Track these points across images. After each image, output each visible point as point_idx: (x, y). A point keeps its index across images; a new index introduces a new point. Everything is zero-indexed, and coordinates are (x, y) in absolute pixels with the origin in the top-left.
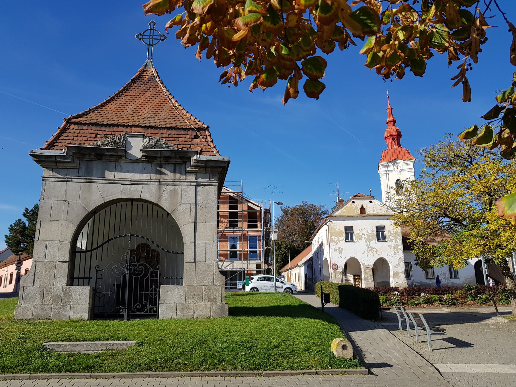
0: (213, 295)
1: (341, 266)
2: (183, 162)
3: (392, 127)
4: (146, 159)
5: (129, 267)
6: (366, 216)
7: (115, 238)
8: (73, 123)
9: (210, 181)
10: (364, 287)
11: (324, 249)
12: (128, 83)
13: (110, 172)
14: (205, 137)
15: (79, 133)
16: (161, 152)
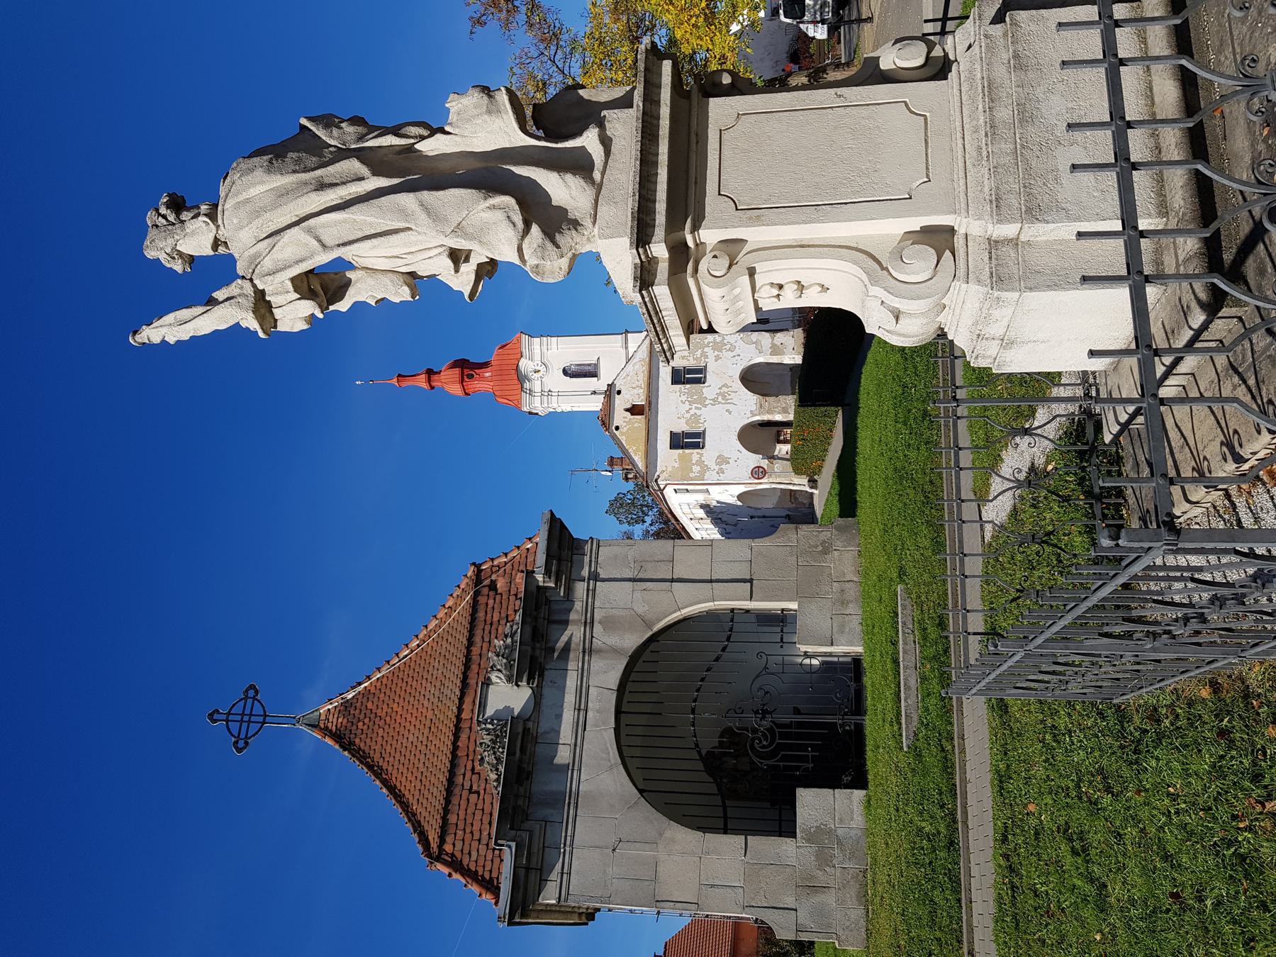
0: (816, 546)
1: (755, 460)
2: (546, 605)
3: (442, 377)
4: (534, 678)
5: (758, 716)
6: (650, 403)
7: (697, 745)
8: (440, 847)
10: (798, 360)
11: (718, 502)
12: (350, 756)
13: (558, 754)
14: (494, 569)
15: (464, 829)
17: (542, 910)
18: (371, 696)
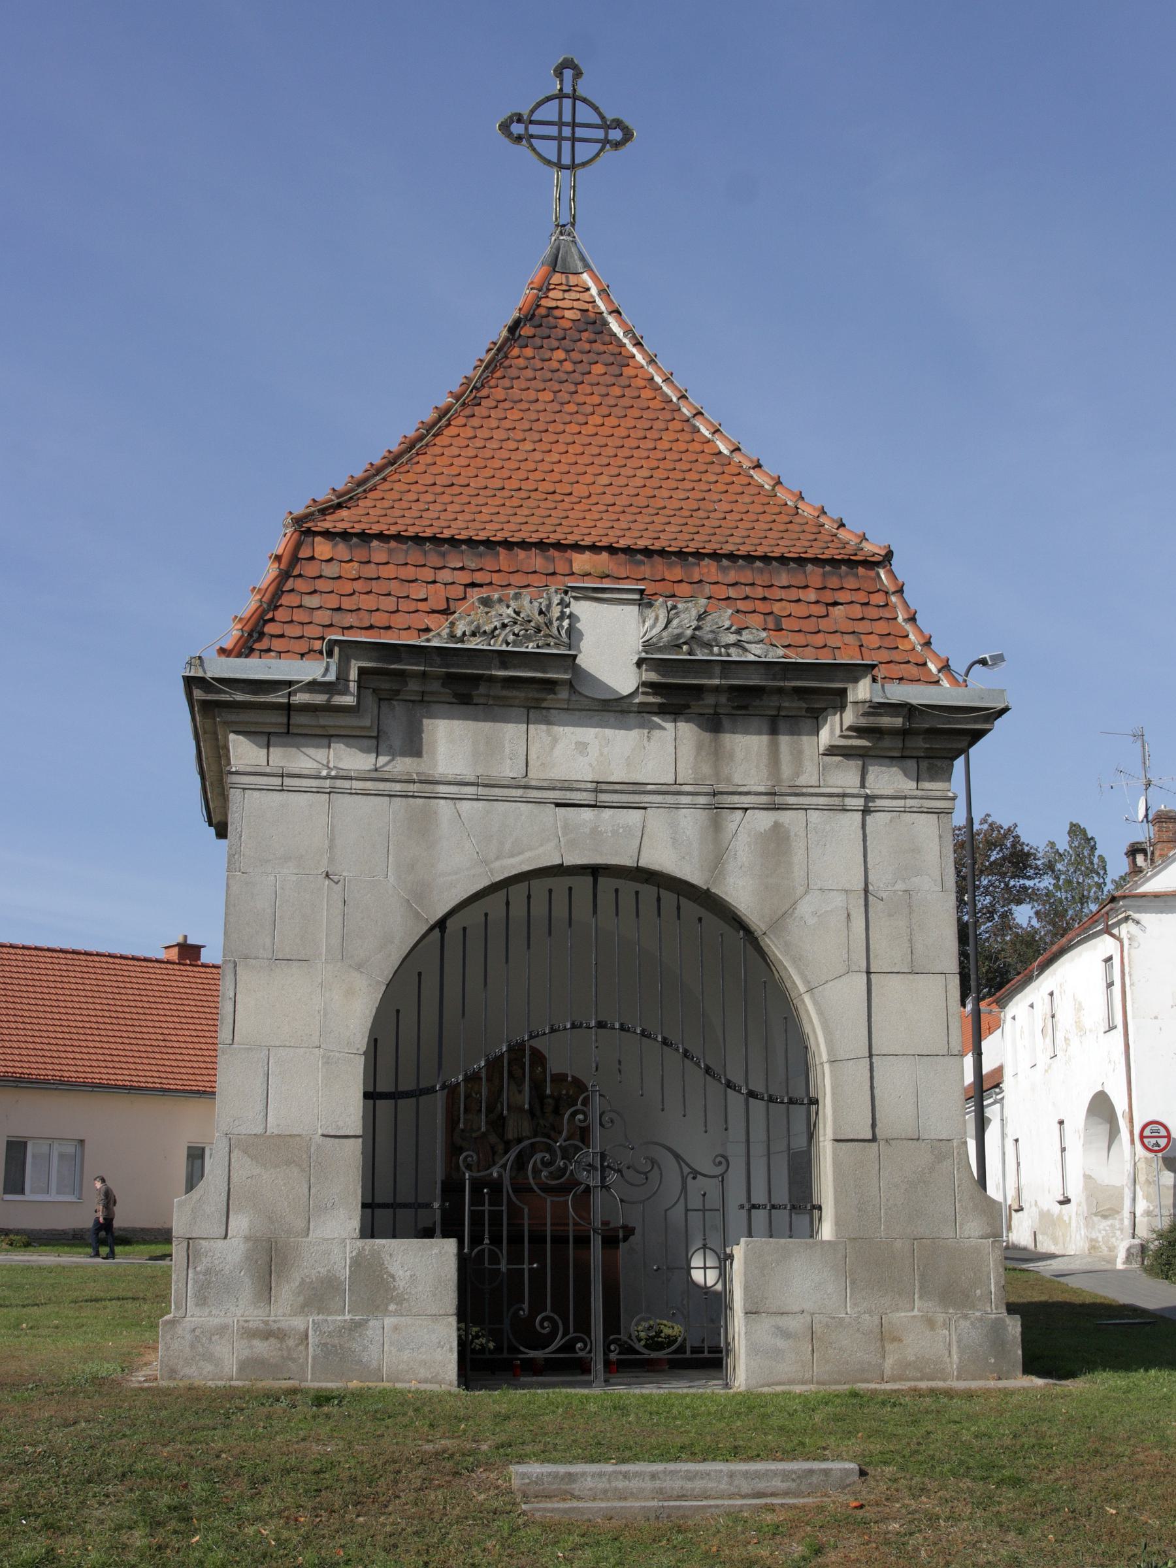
8: (327, 534)
9: (919, 793)
16: (724, 668)
17: (217, 739)
18: (615, 370)
